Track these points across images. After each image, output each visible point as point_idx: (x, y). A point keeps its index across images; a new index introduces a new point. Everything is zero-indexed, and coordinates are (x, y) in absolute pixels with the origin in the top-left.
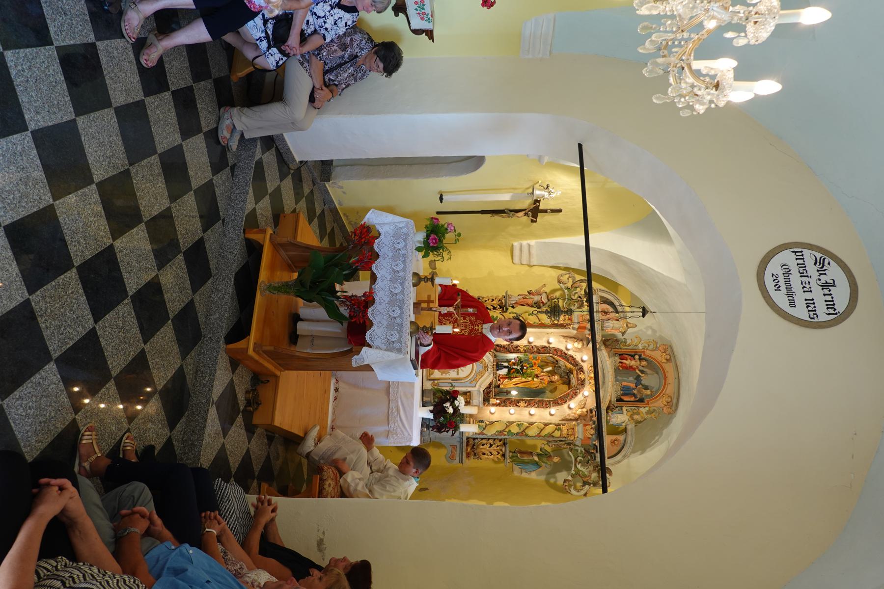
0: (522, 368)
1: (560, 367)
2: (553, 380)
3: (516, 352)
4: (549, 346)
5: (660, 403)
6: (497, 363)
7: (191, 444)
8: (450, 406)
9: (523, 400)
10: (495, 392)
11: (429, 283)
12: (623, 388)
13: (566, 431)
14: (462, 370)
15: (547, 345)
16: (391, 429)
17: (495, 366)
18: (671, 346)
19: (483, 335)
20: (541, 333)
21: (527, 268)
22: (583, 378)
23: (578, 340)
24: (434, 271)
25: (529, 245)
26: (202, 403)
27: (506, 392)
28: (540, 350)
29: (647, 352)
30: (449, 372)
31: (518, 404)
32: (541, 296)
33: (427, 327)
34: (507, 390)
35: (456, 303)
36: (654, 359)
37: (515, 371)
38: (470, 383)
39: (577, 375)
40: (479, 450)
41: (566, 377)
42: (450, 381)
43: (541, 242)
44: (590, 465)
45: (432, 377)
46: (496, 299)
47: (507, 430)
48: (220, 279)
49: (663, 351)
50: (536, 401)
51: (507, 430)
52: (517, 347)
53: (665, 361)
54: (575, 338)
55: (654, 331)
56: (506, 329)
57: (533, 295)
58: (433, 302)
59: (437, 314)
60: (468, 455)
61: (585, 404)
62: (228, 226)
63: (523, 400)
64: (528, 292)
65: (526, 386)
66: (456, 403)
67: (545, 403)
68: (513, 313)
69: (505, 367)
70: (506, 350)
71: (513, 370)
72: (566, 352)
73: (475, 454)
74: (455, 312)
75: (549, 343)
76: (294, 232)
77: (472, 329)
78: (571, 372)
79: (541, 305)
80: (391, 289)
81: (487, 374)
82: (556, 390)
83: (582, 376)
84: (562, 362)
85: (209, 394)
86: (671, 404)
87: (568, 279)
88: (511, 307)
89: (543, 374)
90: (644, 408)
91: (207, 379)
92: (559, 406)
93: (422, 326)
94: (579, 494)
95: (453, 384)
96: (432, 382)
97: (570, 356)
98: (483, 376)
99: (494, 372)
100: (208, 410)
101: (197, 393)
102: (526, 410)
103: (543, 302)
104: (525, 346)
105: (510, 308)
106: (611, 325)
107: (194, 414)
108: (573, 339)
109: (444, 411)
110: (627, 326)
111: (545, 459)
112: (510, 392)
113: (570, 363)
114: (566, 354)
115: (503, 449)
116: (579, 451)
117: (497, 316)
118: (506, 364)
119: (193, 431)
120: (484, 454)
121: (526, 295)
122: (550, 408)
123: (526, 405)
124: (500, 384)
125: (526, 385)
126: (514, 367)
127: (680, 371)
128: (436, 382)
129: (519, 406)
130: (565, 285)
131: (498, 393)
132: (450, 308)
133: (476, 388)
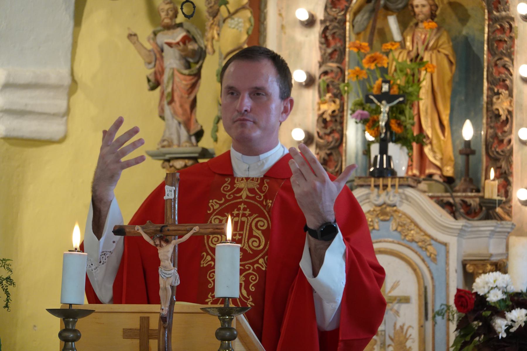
0: (387, 97)
3: (342, 123)
4: (322, 22)
6: (372, 174)
8: (504, 317)
9: (490, 103)
10: (465, 191)
11: (81, 324)
14: (393, 288)
15: (318, 29)
17: (381, 182)
19: (266, 176)
21: (79, 96)
27: (467, 155)
28: (335, 50)
30: (402, 328)
31: (503, 117)
32: (166, 47)
33: (220, 326)
34: (461, 152)
35: (146, 237)
38: (434, 260)
42: (429, 324)
50: (493, 60)
52: (325, 121)
56: (247, 103)
57: (162, 72)
58: (145, 321)
59: (181, 306)
63: (490, 103)
64: (153, 88)
65: (448, 93)
66: (494, 297)
67: (499, 35)
68: (216, 130)
69: (383, 150)
70: (335, 157)
71: (395, 127)
74: (176, 242)
75: (310, 23)
77: (250, 206)
79: (191, 46)
81: (405, 208)
82: (460, 5)
89: (408, 44)
93: (219, 342)
95: (437, 308)
98: (413, 222)
99: (401, 186)
102: (521, 92)
103: (186, 40)
105: (206, 142)
112: (468, 144)
118: (375, 149)
121: (162, 93)
122: (512, 19)
123: (505, 92)
124: (442, 176)
125: (444, 97)
126: (382, 124)
129: (510, 113)
131: (471, 181)
132: (161, 256)
133: (452, 241)
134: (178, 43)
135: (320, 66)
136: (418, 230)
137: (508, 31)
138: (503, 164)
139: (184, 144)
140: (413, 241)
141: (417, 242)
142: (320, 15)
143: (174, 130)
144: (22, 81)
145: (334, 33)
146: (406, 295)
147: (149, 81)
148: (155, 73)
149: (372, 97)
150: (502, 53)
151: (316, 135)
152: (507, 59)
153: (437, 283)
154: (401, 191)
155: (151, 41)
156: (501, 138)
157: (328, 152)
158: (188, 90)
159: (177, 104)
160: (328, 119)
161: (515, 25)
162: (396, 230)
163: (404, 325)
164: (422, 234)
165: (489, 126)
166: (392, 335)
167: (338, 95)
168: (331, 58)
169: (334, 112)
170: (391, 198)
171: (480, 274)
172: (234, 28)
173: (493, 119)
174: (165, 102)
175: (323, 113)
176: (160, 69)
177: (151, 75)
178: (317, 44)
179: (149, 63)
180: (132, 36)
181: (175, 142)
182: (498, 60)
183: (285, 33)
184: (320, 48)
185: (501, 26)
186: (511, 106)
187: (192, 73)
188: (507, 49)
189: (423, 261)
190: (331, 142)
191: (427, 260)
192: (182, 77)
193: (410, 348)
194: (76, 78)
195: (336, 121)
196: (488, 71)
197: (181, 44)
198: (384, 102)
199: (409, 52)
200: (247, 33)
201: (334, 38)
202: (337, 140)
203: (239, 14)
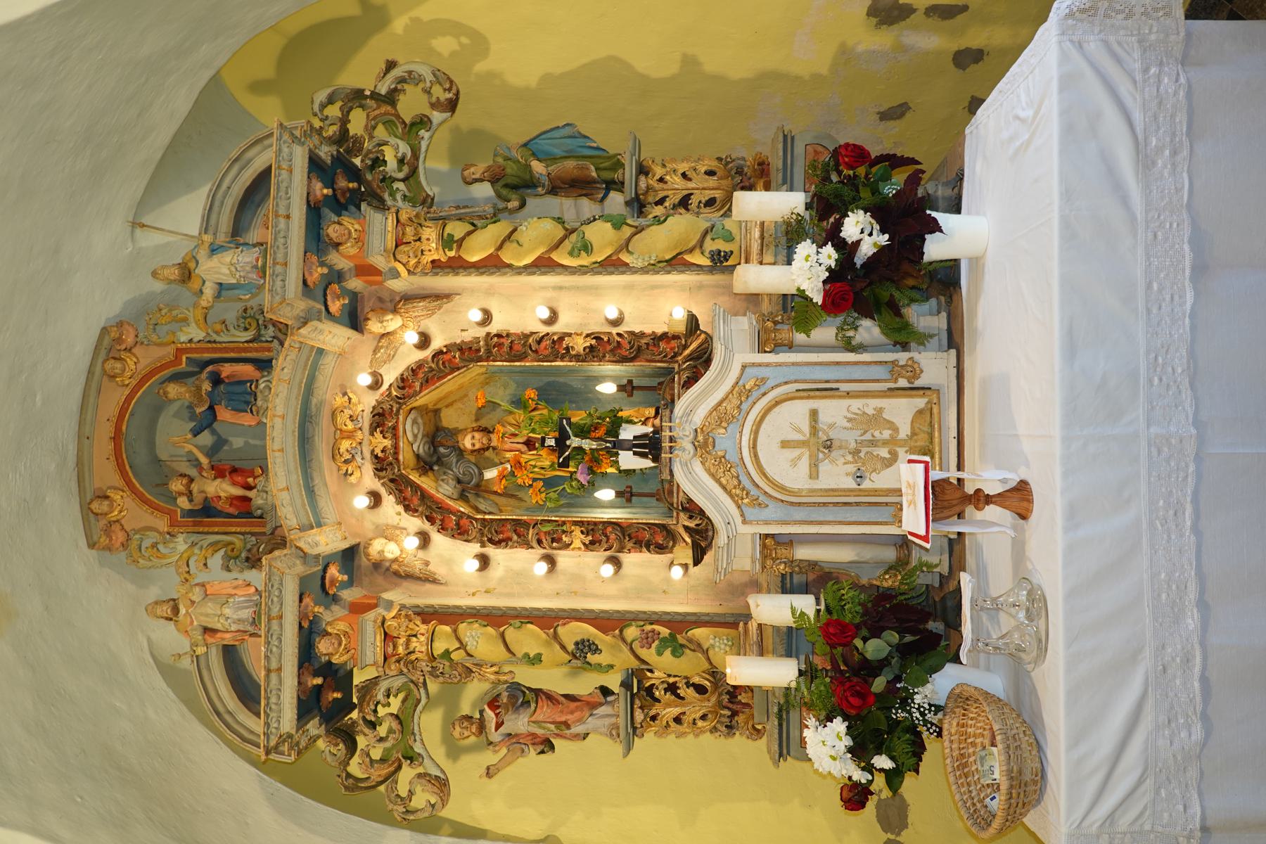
1: (459, 481)
2: (477, 435)
3: (595, 524)
4: (483, 545)
9: (577, 358)
12: (248, 403)
13: (424, 237)
14: (799, 431)
15: (491, 551)
17: (666, 444)
20: (510, 595)
22: (378, 435)
23: (388, 569)
24: (892, 837)
27: (632, 495)
29: (162, 524)
30: (850, 420)
34: (631, 395)
37: (589, 432)
39: (396, 447)
41: (442, 450)
44: (369, 152)
45: (920, 402)
46: (668, 726)
47: (627, 231)
51: (627, 231)
52: (592, 543)
53: (109, 493)
54: (396, 574)
57: (534, 735)
61: (375, 352)
63: (577, 358)
64: (552, 747)
67: (506, 349)
68: (599, 668)
72: (427, 526)
78: (426, 465)
81: (698, 418)
83: (382, 442)
87: (411, 793)
88: (613, 693)
90: (191, 341)
92: (458, 341)
94: (407, 68)
96: (918, 383)
97: (416, 511)
98: (716, 408)
104: (567, 546)
105: (614, 685)
106: (227, 611)
109: (883, 215)
110: (176, 610)
111: (511, 169)
113: (416, 488)
114: (431, 520)
115: (643, 184)
117: (660, 653)
120: (710, 173)
121: (558, 735)
126: (594, 445)
128: (903, 383)
129: (588, 336)
130: (421, 770)
134: (497, 715)
135: (532, 548)
136: (727, 401)
137: (502, 340)
138: (644, 341)
139: (616, 709)
141: (741, 402)
142: (475, 548)
143: (599, 722)
145: (496, 532)
146: (808, 415)
147: (542, 752)
148: (533, 744)
149: (561, 460)
150: (524, 345)
151: (608, 553)
152: (531, 340)
153: (793, 378)
154: (677, 421)
155: (497, 748)
156: (615, 344)
157: (628, 539)
158: (554, 704)
159: (570, 718)
160: (590, 538)
161: (494, 331)
162: (725, 428)
163: (845, 417)
164: (731, 396)
165: (601, 359)
166: (859, 432)
168: (523, 535)
169: (582, 532)
170: (687, 433)
172: (477, 642)
173: (595, 354)
174: (568, 732)
175: (584, 544)
176: (530, 738)
177: (535, 750)
178: (507, 551)
179: (523, 751)
180: (489, 773)
181: (613, 720)
182: (531, 349)
183: (495, 589)
184: (512, 547)
185: (494, 347)
186: (581, 335)
187: (535, 699)
188: (520, 339)
189: (764, 394)
190: (616, 534)
191: (763, 390)
192: (538, 710)
193: (875, 409)
194: (543, 837)
195: (592, 530)
196: (543, 361)
197: (498, 711)
198: (568, 443)
199: (522, 453)
200: (485, 626)
201: (502, 532)
202: (613, 528)
203: (462, 637)
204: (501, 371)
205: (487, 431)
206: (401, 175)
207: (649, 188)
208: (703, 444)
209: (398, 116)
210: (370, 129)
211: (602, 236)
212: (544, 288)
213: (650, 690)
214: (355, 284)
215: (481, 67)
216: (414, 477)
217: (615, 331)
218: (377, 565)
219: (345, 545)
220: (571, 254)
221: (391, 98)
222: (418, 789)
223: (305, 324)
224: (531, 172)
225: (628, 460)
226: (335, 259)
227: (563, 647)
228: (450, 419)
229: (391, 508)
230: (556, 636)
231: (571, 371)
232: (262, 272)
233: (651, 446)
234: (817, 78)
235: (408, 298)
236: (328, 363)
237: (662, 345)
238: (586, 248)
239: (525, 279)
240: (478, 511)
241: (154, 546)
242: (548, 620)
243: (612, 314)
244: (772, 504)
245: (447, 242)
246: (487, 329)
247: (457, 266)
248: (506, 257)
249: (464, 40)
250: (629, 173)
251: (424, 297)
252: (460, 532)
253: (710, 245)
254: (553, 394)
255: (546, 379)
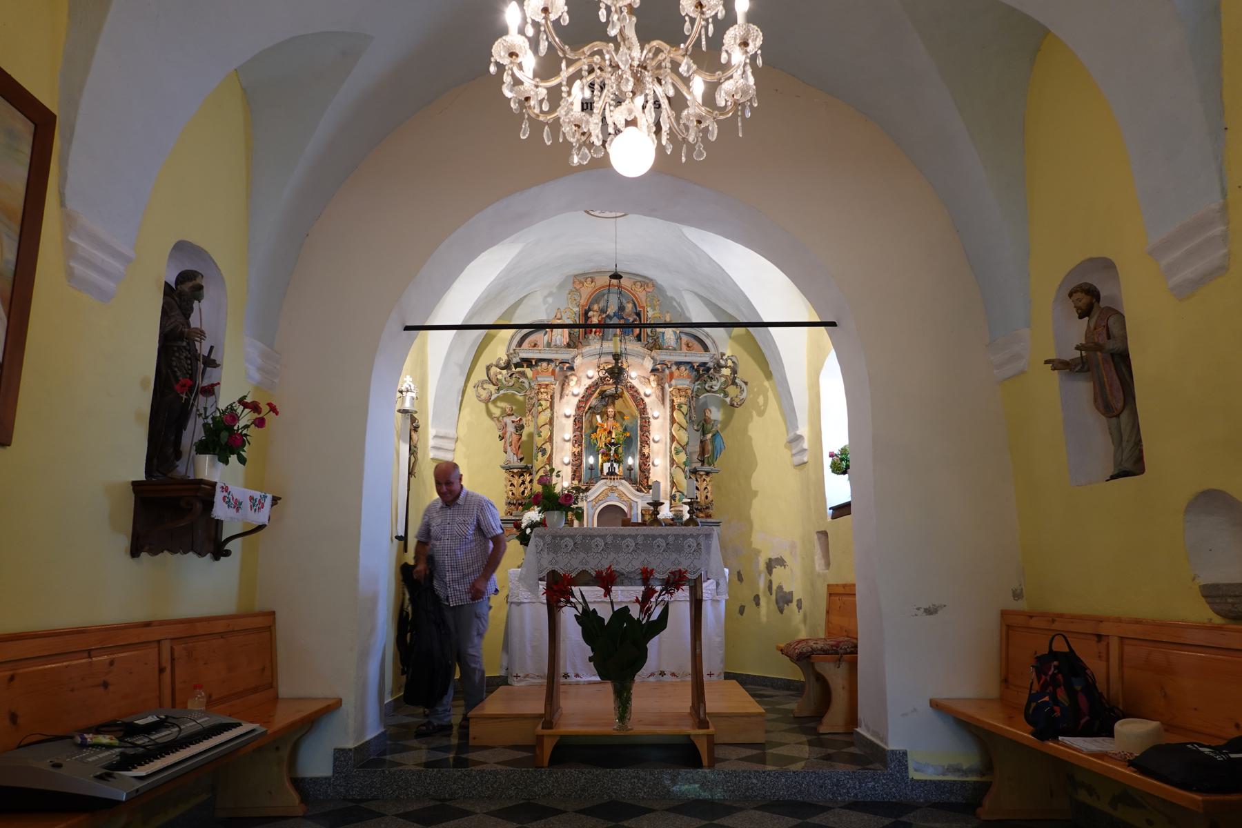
4: (574, 416)
5: (641, 294)
7: (837, 786)
15: (572, 419)
16: (710, 597)
18: (575, 276)
25: (436, 437)
26: (786, 781)
29: (583, 302)
34: (628, 470)
36: (590, 296)
40: (703, 503)
41: (607, 399)
43: (433, 420)
44: (715, 376)
46: (510, 481)
47: (683, 467)
48: (616, 789)
49: (581, 285)
54: (563, 384)
55: (550, 294)
60: (709, 516)
61: (644, 377)
62: (535, 792)
63: (641, 450)
70: (579, 469)
72: (581, 396)
73: (707, 508)
76: (499, 720)
80: (630, 552)
81: (621, 488)
82: (622, 413)
84: (593, 401)
85: (774, 774)
86: (643, 284)
87: (484, 389)
91: (754, 781)
92: (647, 407)
94: (745, 390)
100: (794, 772)
101: (773, 791)
104: (574, 446)
107: (800, 790)
108: (565, 387)
111: (709, 426)
113: (595, 392)
114: (583, 397)
115: (702, 473)
116: (699, 386)
119: (821, 787)
120: (707, 497)
123: (647, 446)
127: (602, 270)
140: (624, 501)
142: (573, 413)
144: (441, 435)
152: (647, 433)
161: (650, 420)
165: (641, 459)
167: (580, 445)
171: (462, 721)
204: (637, 422)
205: (614, 417)
206: (706, 387)
207: (701, 476)
208: (612, 489)
209: (728, 386)
210: (723, 376)
211: (682, 458)
212: (666, 438)
213: (522, 475)
214: (667, 371)
215: (754, 413)
216: (598, 391)
217: (651, 463)
218: (566, 377)
219: (575, 368)
220: (675, 448)
221: (734, 383)
222: (486, 391)
223: (652, 358)
224: (708, 433)
225: (607, 466)
226: (674, 368)
227: (543, 444)
228: (619, 402)
229: (588, 383)
230: (546, 442)
231: (637, 447)
232: (667, 349)
233: (612, 473)
234: (751, 543)
235: (663, 389)
236: (640, 360)
237: (646, 480)
238: (677, 453)
239: (669, 431)
240: (586, 413)
241: (575, 300)
242: (550, 439)
243: (656, 463)
244: (592, 511)
245: (680, 406)
246: (651, 418)
247: (673, 408)
248: (675, 425)
249: (762, 408)
250: (707, 468)
251: (663, 395)
252: (579, 408)
253: (678, 494)
254: (629, 442)
255: (633, 439)
